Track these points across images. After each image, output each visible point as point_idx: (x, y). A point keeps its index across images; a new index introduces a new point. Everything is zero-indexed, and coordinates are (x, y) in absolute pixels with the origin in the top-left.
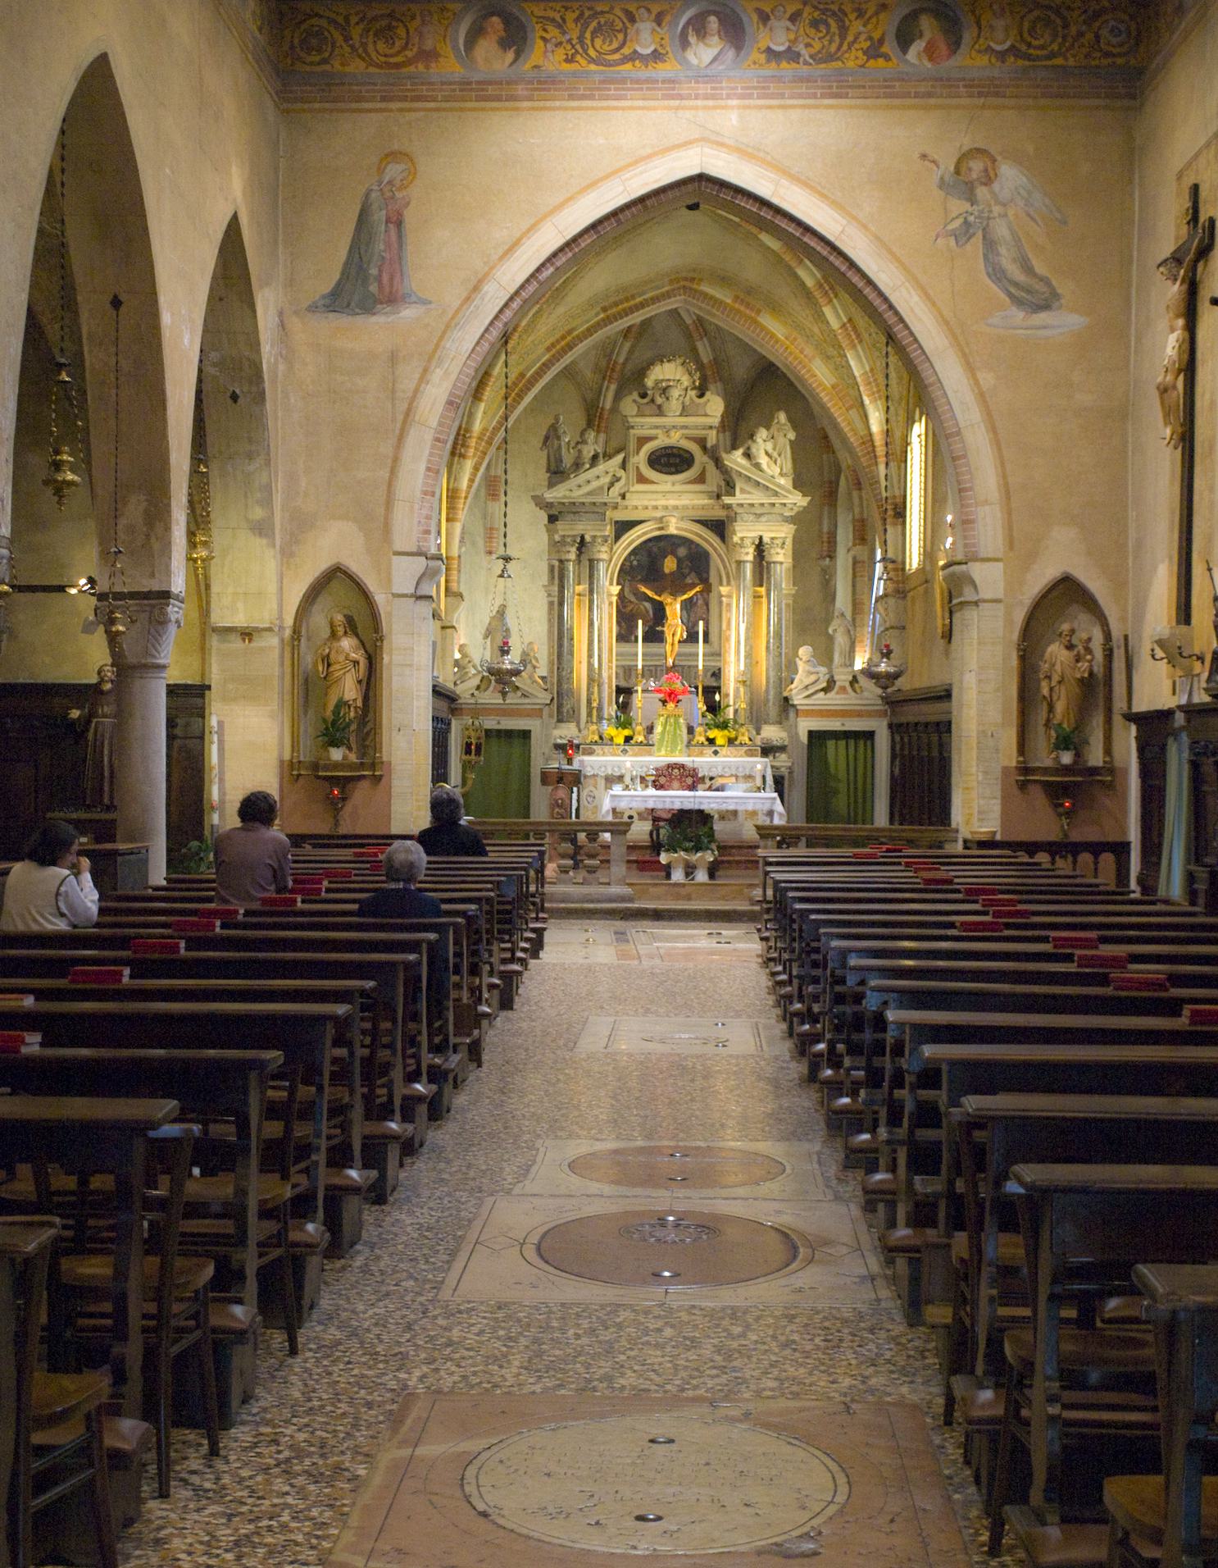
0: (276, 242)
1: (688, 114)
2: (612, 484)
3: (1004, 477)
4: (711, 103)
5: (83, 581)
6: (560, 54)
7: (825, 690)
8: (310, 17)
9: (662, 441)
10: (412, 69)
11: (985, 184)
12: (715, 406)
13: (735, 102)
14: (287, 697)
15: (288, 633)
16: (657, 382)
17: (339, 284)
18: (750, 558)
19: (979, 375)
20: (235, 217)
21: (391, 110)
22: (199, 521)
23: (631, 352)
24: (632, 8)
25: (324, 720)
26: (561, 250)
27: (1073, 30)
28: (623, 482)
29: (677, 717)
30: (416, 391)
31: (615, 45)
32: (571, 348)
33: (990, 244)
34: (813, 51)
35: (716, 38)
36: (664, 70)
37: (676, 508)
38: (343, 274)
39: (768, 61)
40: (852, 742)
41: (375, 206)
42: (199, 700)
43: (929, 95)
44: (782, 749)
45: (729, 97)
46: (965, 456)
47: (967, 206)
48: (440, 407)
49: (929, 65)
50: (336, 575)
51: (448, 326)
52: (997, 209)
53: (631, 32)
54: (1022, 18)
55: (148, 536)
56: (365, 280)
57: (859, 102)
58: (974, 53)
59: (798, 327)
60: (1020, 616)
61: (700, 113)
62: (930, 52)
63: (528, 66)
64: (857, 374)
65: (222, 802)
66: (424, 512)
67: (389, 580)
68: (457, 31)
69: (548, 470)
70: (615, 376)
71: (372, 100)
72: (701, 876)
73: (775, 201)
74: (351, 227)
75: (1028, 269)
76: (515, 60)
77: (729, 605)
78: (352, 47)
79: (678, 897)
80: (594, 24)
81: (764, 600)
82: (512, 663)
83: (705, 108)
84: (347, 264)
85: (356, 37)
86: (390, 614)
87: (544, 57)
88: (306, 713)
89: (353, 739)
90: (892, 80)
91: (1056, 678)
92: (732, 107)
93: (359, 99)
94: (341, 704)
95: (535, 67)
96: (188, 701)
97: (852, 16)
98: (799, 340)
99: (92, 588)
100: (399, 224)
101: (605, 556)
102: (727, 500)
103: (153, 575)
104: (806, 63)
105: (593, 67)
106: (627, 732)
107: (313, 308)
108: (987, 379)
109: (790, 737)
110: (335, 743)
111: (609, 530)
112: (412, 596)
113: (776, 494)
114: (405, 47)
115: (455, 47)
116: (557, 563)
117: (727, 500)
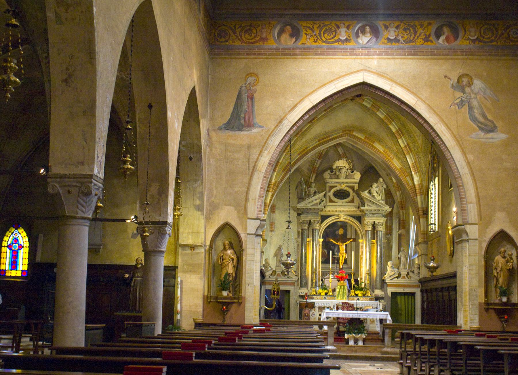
0: (207, 105)
1: (359, 61)
2: (320, 203)
3: (478, 193)
4: (367, 57)
5: (133, 217)
6: (312, 39)
7: (397, 277)
8: (221, 26)
9: (339, 187)
10: (258, 44)
11: (469, 87)
12: (358, 176)
13: (376, 57)
14: (207, 271)
15: (207, 247)
16: (337, 167)
17: (229, 119)
18: (370, 229)
19: (467, 155)
20: (194, 88)
21: (250, 58)
22: (177, 202)
23: (321, 163)
24: (338, 23)
25: (221, 281)
26: (311, 109)
27: (500, 32)
28: (324, 202)
29: (344, 286)
30: (258, 159)
31: (332, 36)
32: (307, 154)
33: (471, 108)
34: (404, 39)
35: (369, 34)
36: (350, 45)
37: (344, 211)
38: (231, 116)
39: (388, 42)
40: (407, 297)
41: (244, 92)
42: (173, 272)
43: (447, 55)
44: (382, 298)
45: (374, 55)
46: (463, 185)
47: (462, 94)
48: (266, 165)
49: (447, 44)
50: (226, 227)
51: (269, 136)
52: (473, 96)
53: (338, 32)
54: (481, 28)
55: (159, 200)
56: (240, 119)
57: (421, 57)
58: (463, 40)
59: (389, 148)
60: (484, 245)
61: (363, 60)
62: (447, 39)
63: (300, 43)
64: (410, 163)
65: (181, 311)
66: (260, 203)
67: (246, 229)
68: (275, 32)
69: (298, 198)
70: (315, 171)
71: (244, 54)
72: (360, 343)
73: (391, 92)
74: (234, 99)
75: (485, 117)
76: (295, 41)
77: (362, 246)
78: (236, 36)
79: (352, 351)
80: (324, 29)
81: (375, 245)
82: (291, 261)
83: (366, 59)
84: (233, 113)
85: (238, 33)
86: (246, 241)
87: (306, 40)
88: (213, 278)
89: (231, 288)
90: (434, 49)
91: (499, 269)
92: (375, 58)
93: (239, 54)
94: (227, 275)
95: (303, 44)
96: (171, 271)
97: (419, 27)
98: (388, 152)
99: (136, 220)
100: (252, 99)
101: (318, 228)
102: (363, 208)
103: (160, 215)
104: (402, 43)
105: (324, 44)
106: (326, 291)
107: (220, 129)
108: (470, 157)
109: (385, 294)
110: (224, 289)
111: (319, 219)
112: (254, 234)
113: (380, 206)
114: (255, 37)
115: (274, 37)
116: (300, 230)
117: (363, 208)
